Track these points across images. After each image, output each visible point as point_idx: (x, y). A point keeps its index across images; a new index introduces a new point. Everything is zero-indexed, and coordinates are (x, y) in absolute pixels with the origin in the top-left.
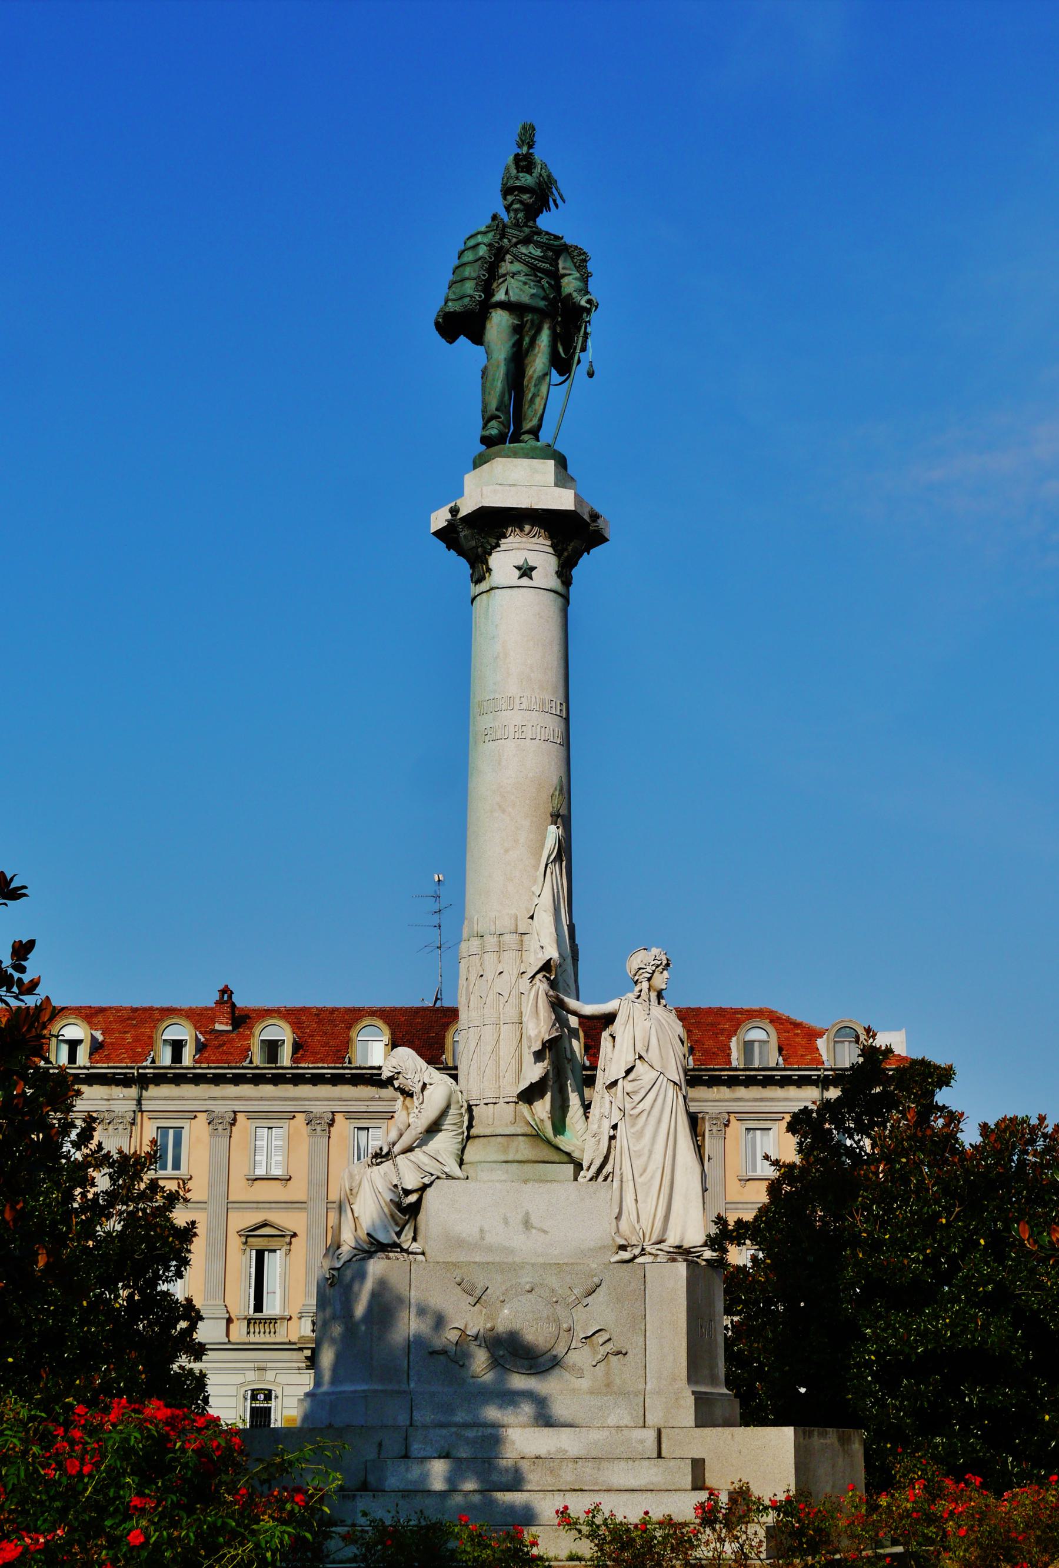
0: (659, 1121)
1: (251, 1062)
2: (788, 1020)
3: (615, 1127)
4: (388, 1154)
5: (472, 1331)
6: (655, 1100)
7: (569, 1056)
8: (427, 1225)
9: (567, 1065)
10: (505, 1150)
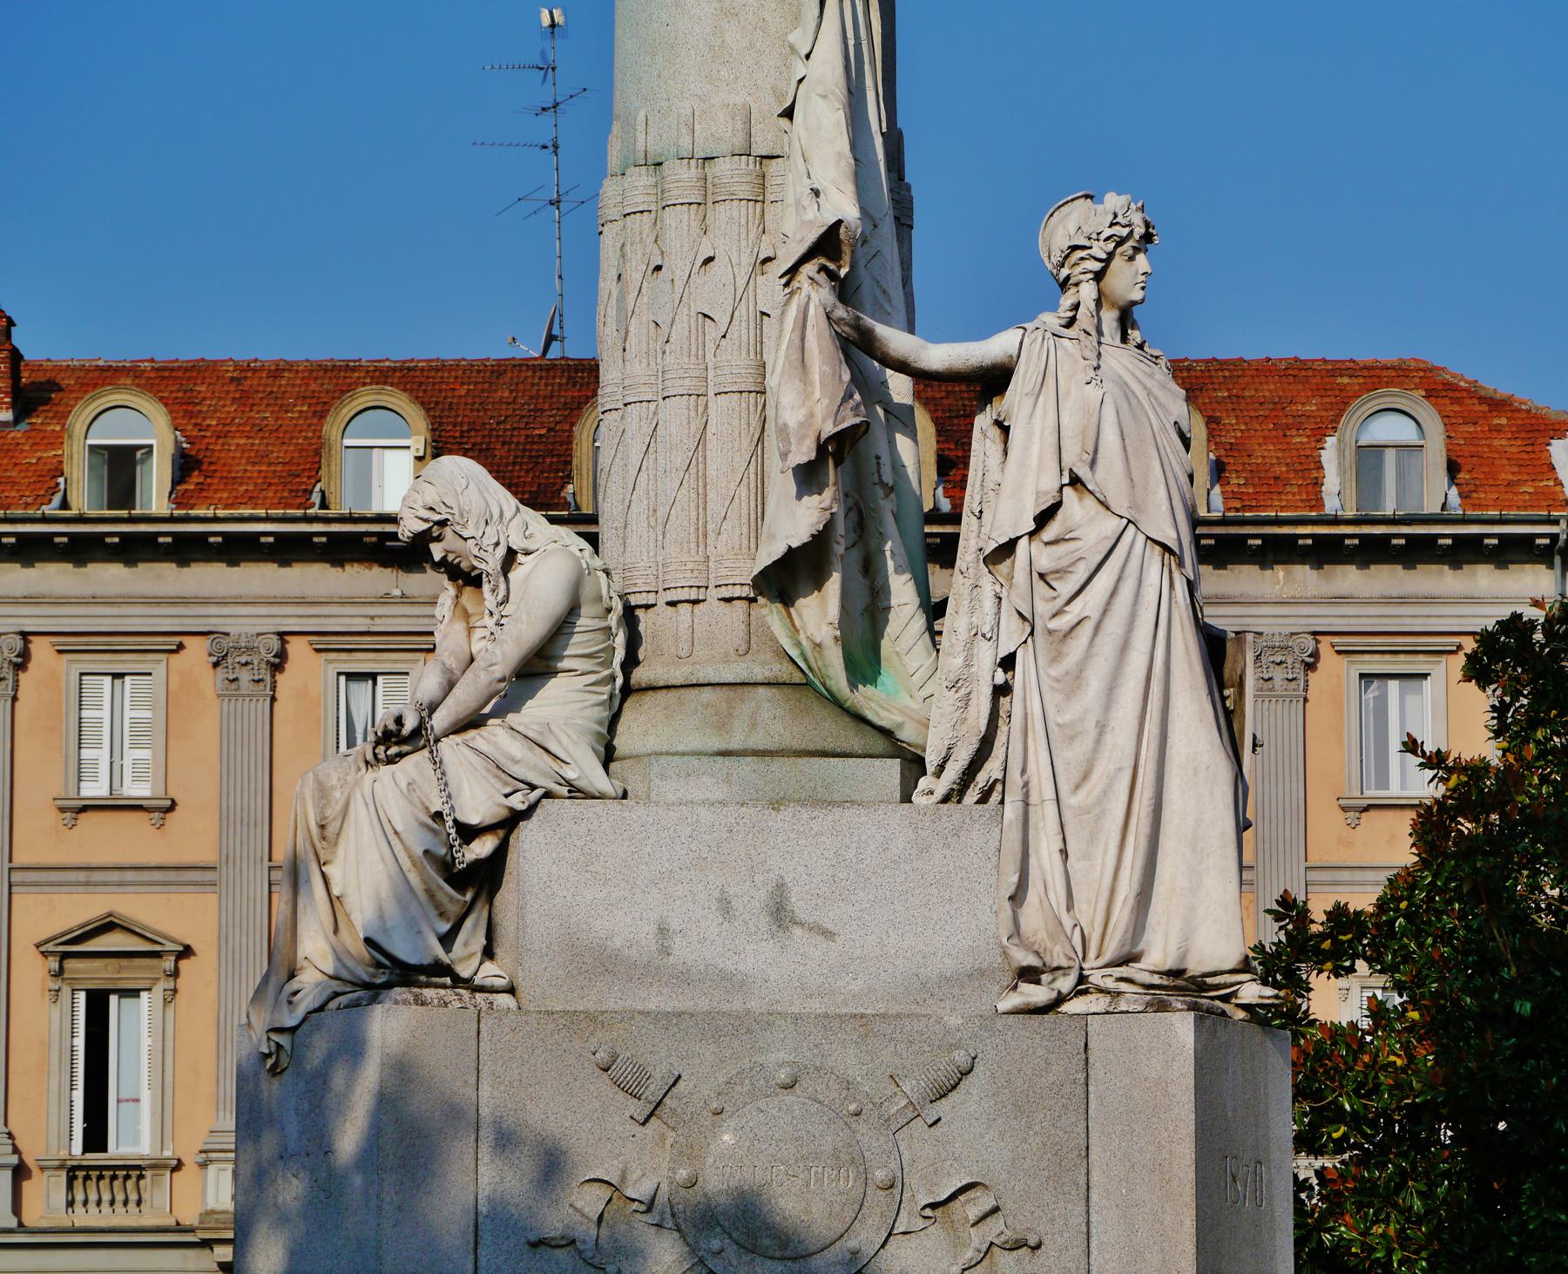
0: (1124, 648)
1: (65, 505)
2: (1473, 393)
3: (1008, 663)
4: (417, 732)
5: (640, 1189)
6: (1114, 593)
7: (888, 477)
8: (521, 916)
9: (880, 509)
10: (722, 726)
